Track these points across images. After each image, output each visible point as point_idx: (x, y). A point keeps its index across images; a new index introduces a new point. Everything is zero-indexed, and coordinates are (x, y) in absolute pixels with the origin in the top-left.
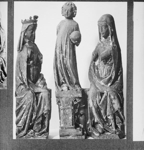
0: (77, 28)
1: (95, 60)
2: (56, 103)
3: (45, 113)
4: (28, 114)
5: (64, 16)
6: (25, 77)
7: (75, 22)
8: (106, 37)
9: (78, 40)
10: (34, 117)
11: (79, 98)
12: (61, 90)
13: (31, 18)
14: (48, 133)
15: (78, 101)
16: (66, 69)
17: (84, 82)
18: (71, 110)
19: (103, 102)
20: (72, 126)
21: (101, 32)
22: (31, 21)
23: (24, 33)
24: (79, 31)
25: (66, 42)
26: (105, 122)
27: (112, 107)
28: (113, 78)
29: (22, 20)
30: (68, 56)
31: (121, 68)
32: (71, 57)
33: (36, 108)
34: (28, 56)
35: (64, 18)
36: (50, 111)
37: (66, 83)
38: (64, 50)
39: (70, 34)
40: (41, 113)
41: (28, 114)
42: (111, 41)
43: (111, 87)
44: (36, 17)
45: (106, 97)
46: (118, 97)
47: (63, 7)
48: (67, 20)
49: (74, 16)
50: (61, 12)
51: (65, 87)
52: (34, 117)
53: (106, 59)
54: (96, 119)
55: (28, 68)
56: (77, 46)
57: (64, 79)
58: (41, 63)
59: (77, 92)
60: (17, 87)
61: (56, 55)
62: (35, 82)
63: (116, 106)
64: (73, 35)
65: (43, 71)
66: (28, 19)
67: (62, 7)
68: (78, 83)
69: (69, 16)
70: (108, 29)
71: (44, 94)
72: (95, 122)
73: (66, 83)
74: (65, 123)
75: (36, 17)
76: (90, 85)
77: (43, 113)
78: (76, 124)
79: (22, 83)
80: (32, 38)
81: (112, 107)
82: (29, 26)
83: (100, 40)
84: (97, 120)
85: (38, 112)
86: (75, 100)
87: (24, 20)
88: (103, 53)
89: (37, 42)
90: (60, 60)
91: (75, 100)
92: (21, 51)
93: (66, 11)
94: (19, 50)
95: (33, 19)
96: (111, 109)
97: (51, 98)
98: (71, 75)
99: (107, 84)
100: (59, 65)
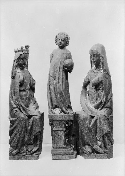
0: (69, 57)
1: (85, 86)
2: (49, 124)
5: (57, 45)
7: (68, 51)
11: (71, 121)
13: (22, 48)
14: (69, 158)
19: (93, 126)
21: (92, 60)
22: (22, 50)
25: (60, 69)
28: (103, 102)
30: (60, 82)
32: (64, 83)
34: (20, 82)
38: (57, 76)
42: (102, 68)
47: (56, 37)
50: (54, 41)
56: (70, 72)
60: (111, 99)
66: (20, 49)
67: (56, 36)
75: (27, 47)
83: (91, 67)
85: (30, 134)
88: (94, 80)
91: (67, 123)
95: (24, 48)
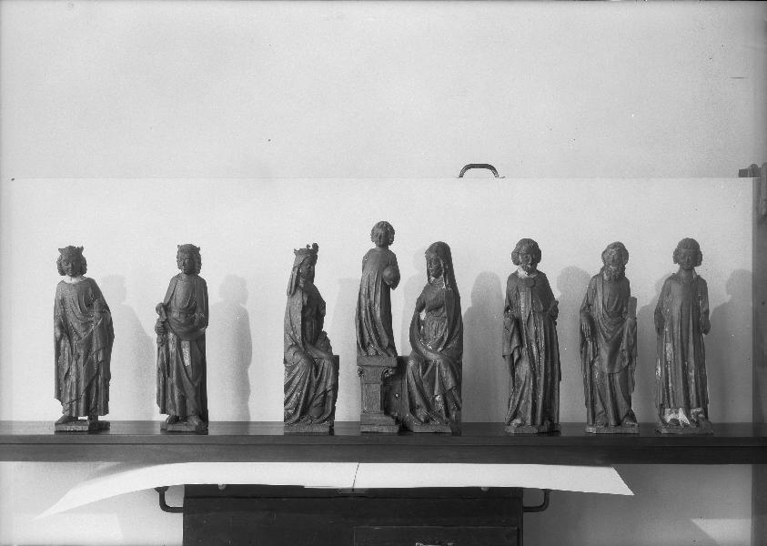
1: (419, 309)
4: (302, 389)
6: (299, 336)
8: (437, 276)
9: (395, 280)
10: (311, 396)
13: (308, 246)
16: (374, 322)
17: (403, 346)
18: (379, 386)
26: (429, 405)
27: (442, 384)
31: (459, 321)
36: (335, 387)
37: (373, 343)
40: (321, 390)
41: (302, 389)
46: (452, 368)
49: (390, 244)
52: (311, 396)
53: (434, 309)
54: (418, 401)
55: (304, 320)
57: (371, 338)
58: (683, 251)
62: (313, 343)
63: (450, 383)
65: (328, 326)
68: (392, 346)
74: (370, 406)
76: (656, 334)
78: (387, 408)
80: (310, 276)
81: (442, 384)
85: (317, 387)
89: (316, 283)
92: (294, 294)
95: (311, 248)
97: (109, 378)
98: (383, 333)
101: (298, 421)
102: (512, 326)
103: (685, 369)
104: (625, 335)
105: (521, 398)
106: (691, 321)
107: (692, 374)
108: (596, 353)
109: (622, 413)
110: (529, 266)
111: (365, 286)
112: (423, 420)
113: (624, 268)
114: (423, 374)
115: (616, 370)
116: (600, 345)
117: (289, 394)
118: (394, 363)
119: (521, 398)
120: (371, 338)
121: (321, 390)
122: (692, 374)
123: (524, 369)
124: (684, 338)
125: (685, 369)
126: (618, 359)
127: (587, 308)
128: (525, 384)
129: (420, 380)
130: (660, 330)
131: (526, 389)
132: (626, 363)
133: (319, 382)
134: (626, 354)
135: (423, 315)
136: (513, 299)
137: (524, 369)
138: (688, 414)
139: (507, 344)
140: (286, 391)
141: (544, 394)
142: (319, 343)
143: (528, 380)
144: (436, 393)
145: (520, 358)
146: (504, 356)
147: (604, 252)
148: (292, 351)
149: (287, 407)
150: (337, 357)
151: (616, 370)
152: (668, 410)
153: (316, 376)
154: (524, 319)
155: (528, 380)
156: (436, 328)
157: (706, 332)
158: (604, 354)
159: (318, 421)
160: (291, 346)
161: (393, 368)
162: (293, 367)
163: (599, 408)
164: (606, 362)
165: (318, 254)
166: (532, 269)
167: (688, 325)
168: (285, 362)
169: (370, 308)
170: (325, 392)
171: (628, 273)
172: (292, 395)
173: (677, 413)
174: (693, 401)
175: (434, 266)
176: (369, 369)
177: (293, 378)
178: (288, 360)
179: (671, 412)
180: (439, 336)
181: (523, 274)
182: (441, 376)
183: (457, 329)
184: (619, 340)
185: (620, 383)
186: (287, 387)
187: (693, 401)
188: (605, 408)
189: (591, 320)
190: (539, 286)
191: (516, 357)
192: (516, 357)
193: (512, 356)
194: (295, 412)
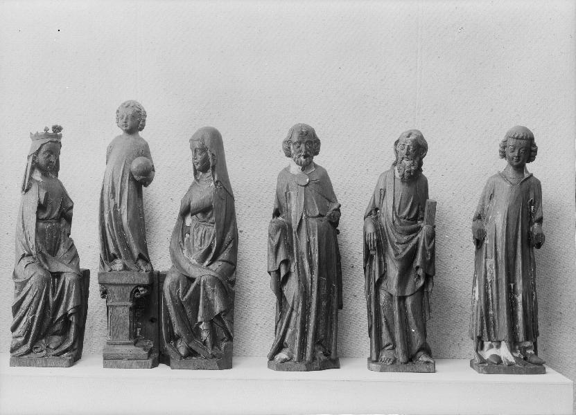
2: (99, 294)
3: (69, 313)
12: (109, 269)
13: (46, 130)
15: (142, 291)
17: (162, 261)
18: (127, 310)
20: (128, 341)
22: (47, 135)
23: (34, 158)
24: (150, 158)
27: (209, 306)
29: (31, 133)
33: (52, 300)
34: (39, 201)
35: (121, 132)
39: (131, 162)
40: (60, 314)
43: (211, 267)
44: (57, 129)
45: (198, 285)
47: (118, 111)
48: (126, 136)
51: (118, 265)
59: (140, 275)
61: (102, 202)
62: (54, 251)
63: (218, 307)
64: (136, 164)
66: (42, 131)
68: (144, 258)
69: (128, 128)
70: (207, 156)
71: (69, 278)
72: (173, 333)
73: (120, 257)
76: (474, 247)
77: (67, 313)
79: (26, 253)
82: (42, 145)
84: (178, 331)
86: (138, 291)
87: (34, 133)
90: (110, 215)
92: (27, 191)
93: (122, 118)
94: (23, 190)
95: (51, 131)
96: (514, 286)
99: (203, 261)
100: (107, 222)
101: (28, 352)
102: (279, 233)
103: (511, 292)
104: (420, 249)
105: (287, 326)
106: (520, 231)
107: (520, 298)
108: (383, 275)
109: (417, 342)
110: (302, 158)
111: (108, 181)
112: (183, 353)
113: (420, 164)
114: (185, 293)
115: (408, 292)
116: (389, 261)
117: (17, 318)
118: (146, 281)
119: (287, 326)
120: (117, 249)
121: (60, 314)
122: (520, 298)
123: (292, 289)
124: (511, 254)
125: (511, 292)
126: (412, 279)
127: (374, 212)
128: (292, 309)
129: (180, 302)
130: (479, 242)
131: (294, 314)
132: (422, 282)
133: (58, 304)
134: (420, 272)
135: (189, 221)
136: (283, 201)
137: (292, 289)
138: (512, 350)
139: (272, 256)
140: (14, 315)
141: (317, 316)
142: (424, 346)
143: (296, 303)
144: (199, 319)
145: (288, 274)
146: (269, 273)
147: (396, 143)
148: (24, 262)
149: (16, 333)
150: (103, 297)
151: (408, 292)
152: (487, 344)
153: (53, 296)
154: (295, 226)
155: (296, 303)
156: (203, 233)
157: (539, 246)
158: (393, 271)
159: (55, 352)
160: (24, 256)
161: (145, 286)
162: (24, 284)
163: (385, 338)
164: (395, 282)
165: (63, 141)
166: (307, 166)
167: (516, 236)
168: (15, 276)
169: (116, 212)
170: (66, 316)
171: (426, 171)
172: (21, 319)
173: (498, 347)
174: (521, 336)
175: (199, 158)
176: (113, 288)
177: (23, 298)
178: (17, 272)
179: (491, 347)
180: (205, 247)
181: (295, 169)
182: (206, 295)
183: (229, 237)
184: (412, 255)
185: (414, 313)
186: (16, 308)
187: (521, 336)
188: (393, 339)
189: (379, 231)
190: (322, 190)
191: (283, 273)
192: (283, 273)
193: (278, 272)
194: (25, 342)
